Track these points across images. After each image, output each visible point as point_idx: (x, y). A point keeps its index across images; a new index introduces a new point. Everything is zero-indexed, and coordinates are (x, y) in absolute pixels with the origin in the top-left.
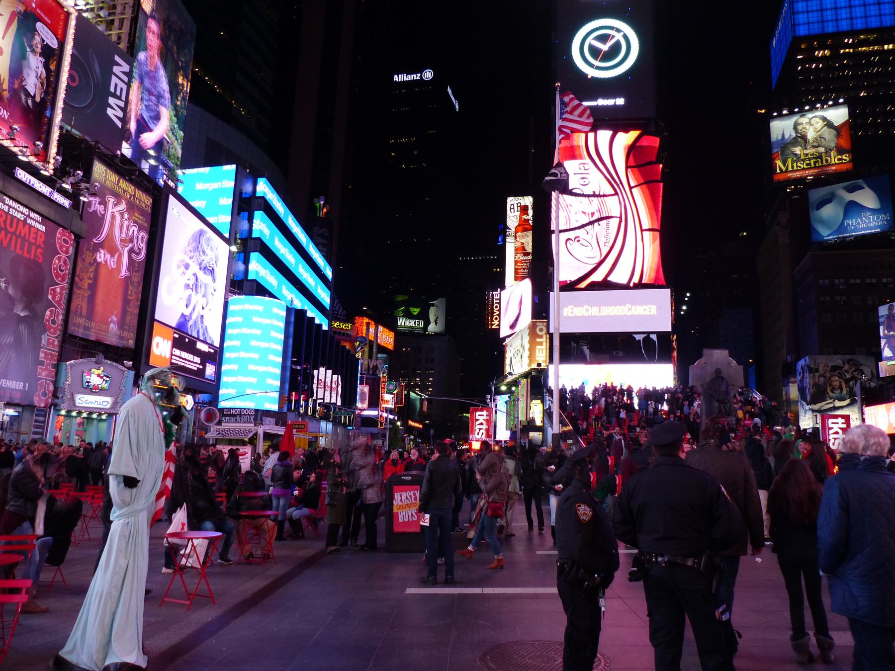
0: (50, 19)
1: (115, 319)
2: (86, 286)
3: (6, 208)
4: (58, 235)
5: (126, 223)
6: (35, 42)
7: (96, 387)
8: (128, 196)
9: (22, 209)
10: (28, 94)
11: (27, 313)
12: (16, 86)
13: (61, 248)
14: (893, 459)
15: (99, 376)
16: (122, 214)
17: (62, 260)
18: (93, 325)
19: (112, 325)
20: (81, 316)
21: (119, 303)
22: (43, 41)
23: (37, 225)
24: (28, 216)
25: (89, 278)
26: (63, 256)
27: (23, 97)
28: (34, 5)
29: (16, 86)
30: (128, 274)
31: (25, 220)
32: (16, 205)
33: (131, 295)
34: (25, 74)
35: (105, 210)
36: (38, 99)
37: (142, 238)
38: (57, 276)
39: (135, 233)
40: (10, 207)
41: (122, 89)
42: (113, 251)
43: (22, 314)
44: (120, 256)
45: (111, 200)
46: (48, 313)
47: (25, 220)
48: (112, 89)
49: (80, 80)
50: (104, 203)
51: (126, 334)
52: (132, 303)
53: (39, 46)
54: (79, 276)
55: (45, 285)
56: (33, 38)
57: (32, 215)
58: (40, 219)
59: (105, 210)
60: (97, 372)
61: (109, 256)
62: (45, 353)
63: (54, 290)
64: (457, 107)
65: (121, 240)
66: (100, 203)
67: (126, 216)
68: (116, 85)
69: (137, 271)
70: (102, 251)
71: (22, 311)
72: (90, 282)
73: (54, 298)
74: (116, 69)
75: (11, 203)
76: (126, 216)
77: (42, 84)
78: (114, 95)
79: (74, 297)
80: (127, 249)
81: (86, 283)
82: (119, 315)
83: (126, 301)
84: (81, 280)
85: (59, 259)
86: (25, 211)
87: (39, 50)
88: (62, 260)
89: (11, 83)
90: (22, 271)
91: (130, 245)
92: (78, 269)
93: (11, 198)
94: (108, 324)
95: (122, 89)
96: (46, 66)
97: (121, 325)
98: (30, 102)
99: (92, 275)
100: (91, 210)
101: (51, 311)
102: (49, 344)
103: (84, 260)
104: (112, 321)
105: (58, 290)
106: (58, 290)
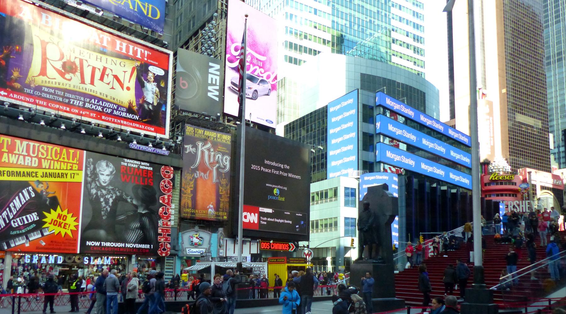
0: (156, 62)
1: (212, 206)
2: (189, 192)
3: (126, 164)
4: (162, 170)
5: (212, 153)
6: (149, 77)
7: (196, 244)
8: (212, 138)
9: (135, 162)
10: (148, 104)
11: (147, 211)
12: (141, 102)
13: (165, 175)
14: (559, 124)
15: (197, 238)
16: (209, 150)
17: (166, 182)
18: (197, 211)
19: (210, 210)
20: (188, 208)
21: (214, 197)
22: (154, 74)
23: (146, 168)
24: (141, 165)
25: (191, 188)
26: (167, 180)
27: (146, 106)
28: (146, 59)
29: (141, 102)
30: (217, 181)
31: (139, 167)
32: (132, 161)
33: (222, 192)
34: (145, 94)
35: (196, 150)
36: (155, 104)
37: (226, 159)
38: (164, 190)
39: (220, 158)
40: (128, 163)
41: (216, 80)
42: (205, 170)
43: (144, 212)
44: (211, 172)
45: (200, 144)
46: (161, 209)
47: (139, 167)
48: (210, 82)
49: (189, 84)
50: (195, 146)
51: (221, 213)
52: (223, 196)
53: (152, 78)
54: (184, 188)
55: (157, 196)
56: (148, 75)
57: (143, 163)
58: (148, 165)
59: (196, 150)
60: (196, 236)
61: (203, 174)
62: (162, 229)
63: (164, 198)
64: (395, 226)
65: (210, 164)
66: (192, 147)
67: (212, 150)
68: (212, 79)
69: (224, 179)
70: (198, 172)
71: (143, 210)
72: (192, 189)
73: (164, 201)
74: (211, 70)
75: (128, 161)
76: (212, 150)
77: (157, 96)
78: (212, 84)
79: (182, 199)
80: (215, 168)
81: (189, 191)
82: (215, 205)
83: (218, 196)
84: (186, 189)
85: (164, 182)
86: (138, 163)
87: (152, 79)
88: (166, 182)
89: (137, 101)
90: (140, 192)
91: (217, 165)
92: (183, 184)
93: (128, 158)
94: (208, 209)
95: (216, 80)
96: (158, 86)
97: (217, 209)
98: (150, 107)
99: (192, 186)
100: (187, 152)
101: (163, 208)
102: (163, 224)
103: (186, 179)
104: (210, 208)
105: (166, 197)
106: (166, 197)
